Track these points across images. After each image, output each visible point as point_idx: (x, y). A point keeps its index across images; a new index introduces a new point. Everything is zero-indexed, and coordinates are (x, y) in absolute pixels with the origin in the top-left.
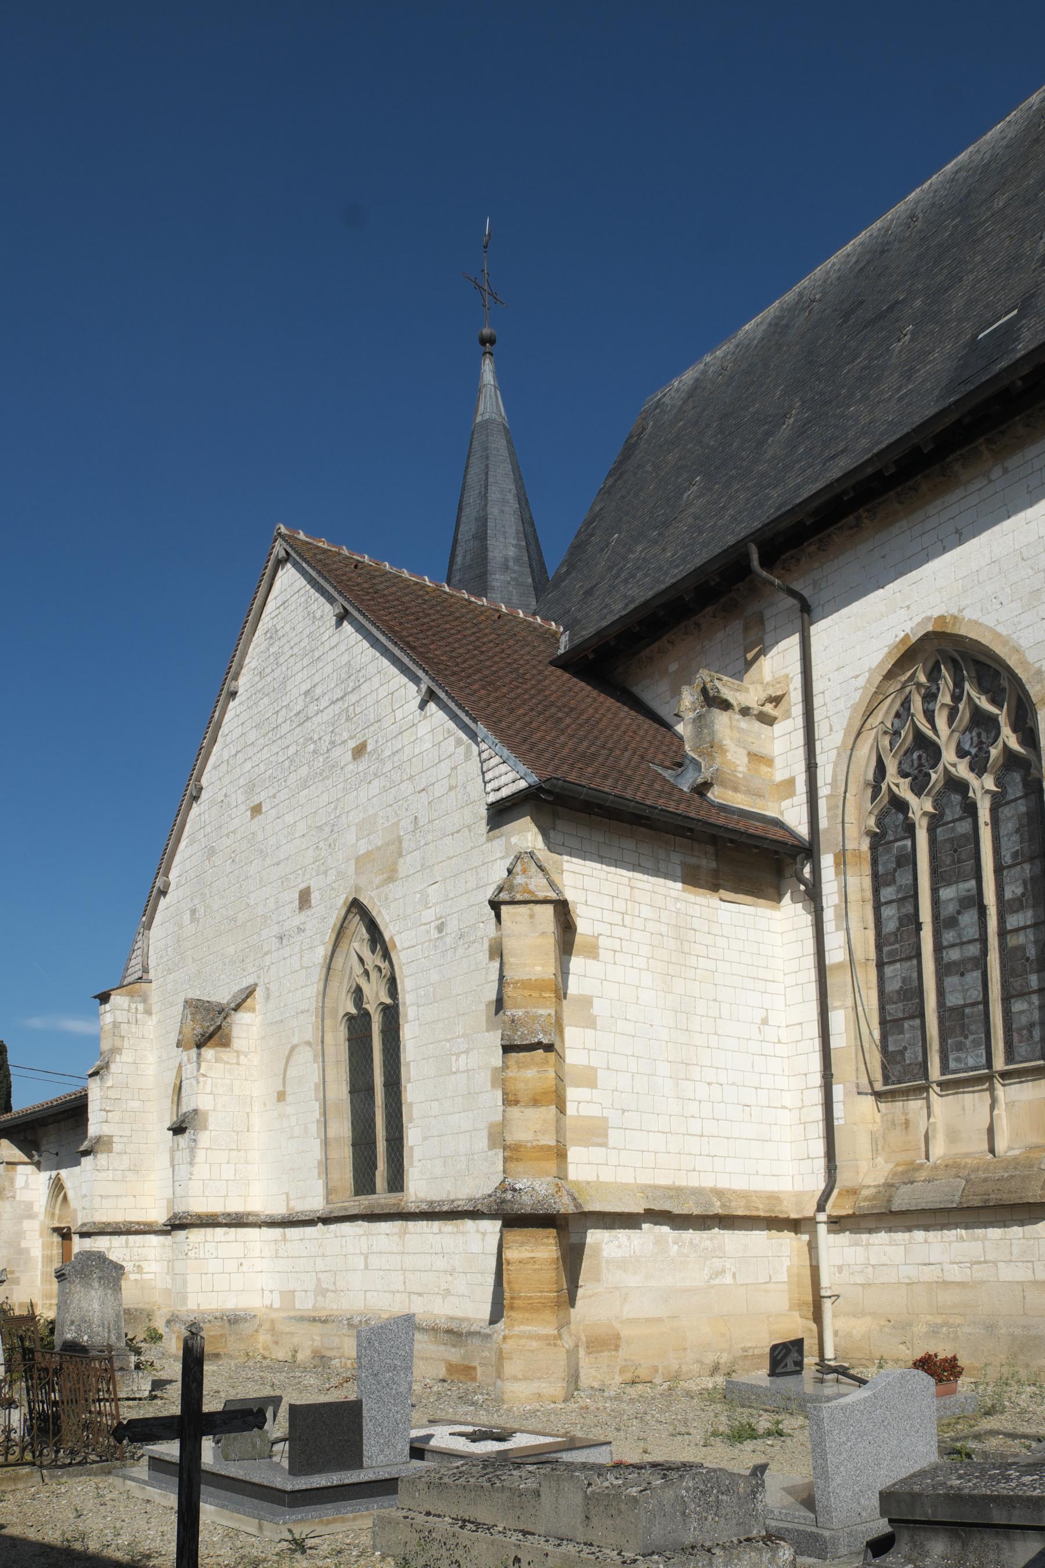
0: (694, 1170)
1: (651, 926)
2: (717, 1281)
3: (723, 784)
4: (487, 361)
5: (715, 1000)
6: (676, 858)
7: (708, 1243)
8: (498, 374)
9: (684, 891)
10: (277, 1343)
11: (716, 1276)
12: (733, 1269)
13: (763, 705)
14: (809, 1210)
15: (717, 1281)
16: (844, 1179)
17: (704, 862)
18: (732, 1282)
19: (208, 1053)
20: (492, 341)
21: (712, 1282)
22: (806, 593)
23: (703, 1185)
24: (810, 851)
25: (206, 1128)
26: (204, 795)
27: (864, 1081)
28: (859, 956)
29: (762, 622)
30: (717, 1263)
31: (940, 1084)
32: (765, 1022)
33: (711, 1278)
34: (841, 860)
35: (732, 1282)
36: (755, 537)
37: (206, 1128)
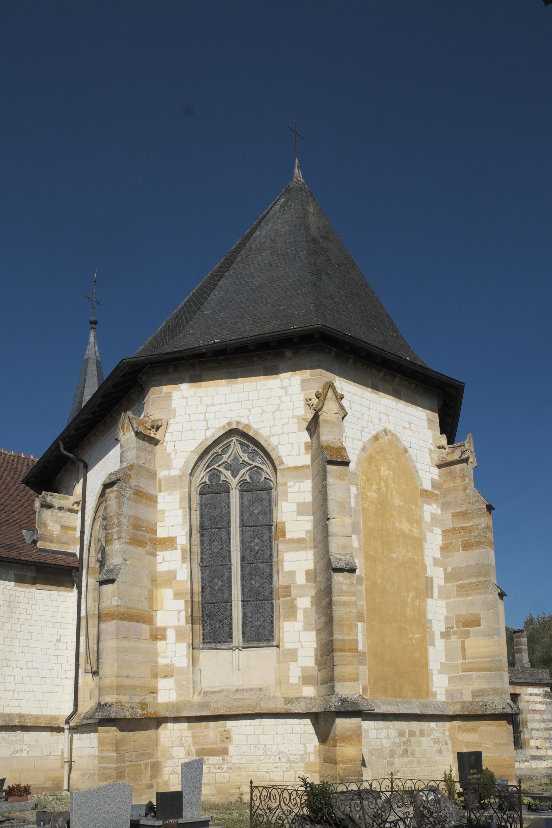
0: (8, 706)
2: (17, 755)
3: (44, 540)
4: (92, 332)
5: (29, 632)
6: (12, 573)
7: (13, 738)
8: (96, 337)
9: (15, 586)
11: (17, 753)
12: (28, 749)
13: (73, 505)
15: (17, 755)
17: (29, 574)
18: (26, 755)
20: (95, 323)
21: (14, 755)
22: (86, 461)
23: (13, 712)
24: (79, 569)
27: (89, 667)
30: (18, 747)
33: (13, 753)
35: (26, 755)
36: (62, 438)
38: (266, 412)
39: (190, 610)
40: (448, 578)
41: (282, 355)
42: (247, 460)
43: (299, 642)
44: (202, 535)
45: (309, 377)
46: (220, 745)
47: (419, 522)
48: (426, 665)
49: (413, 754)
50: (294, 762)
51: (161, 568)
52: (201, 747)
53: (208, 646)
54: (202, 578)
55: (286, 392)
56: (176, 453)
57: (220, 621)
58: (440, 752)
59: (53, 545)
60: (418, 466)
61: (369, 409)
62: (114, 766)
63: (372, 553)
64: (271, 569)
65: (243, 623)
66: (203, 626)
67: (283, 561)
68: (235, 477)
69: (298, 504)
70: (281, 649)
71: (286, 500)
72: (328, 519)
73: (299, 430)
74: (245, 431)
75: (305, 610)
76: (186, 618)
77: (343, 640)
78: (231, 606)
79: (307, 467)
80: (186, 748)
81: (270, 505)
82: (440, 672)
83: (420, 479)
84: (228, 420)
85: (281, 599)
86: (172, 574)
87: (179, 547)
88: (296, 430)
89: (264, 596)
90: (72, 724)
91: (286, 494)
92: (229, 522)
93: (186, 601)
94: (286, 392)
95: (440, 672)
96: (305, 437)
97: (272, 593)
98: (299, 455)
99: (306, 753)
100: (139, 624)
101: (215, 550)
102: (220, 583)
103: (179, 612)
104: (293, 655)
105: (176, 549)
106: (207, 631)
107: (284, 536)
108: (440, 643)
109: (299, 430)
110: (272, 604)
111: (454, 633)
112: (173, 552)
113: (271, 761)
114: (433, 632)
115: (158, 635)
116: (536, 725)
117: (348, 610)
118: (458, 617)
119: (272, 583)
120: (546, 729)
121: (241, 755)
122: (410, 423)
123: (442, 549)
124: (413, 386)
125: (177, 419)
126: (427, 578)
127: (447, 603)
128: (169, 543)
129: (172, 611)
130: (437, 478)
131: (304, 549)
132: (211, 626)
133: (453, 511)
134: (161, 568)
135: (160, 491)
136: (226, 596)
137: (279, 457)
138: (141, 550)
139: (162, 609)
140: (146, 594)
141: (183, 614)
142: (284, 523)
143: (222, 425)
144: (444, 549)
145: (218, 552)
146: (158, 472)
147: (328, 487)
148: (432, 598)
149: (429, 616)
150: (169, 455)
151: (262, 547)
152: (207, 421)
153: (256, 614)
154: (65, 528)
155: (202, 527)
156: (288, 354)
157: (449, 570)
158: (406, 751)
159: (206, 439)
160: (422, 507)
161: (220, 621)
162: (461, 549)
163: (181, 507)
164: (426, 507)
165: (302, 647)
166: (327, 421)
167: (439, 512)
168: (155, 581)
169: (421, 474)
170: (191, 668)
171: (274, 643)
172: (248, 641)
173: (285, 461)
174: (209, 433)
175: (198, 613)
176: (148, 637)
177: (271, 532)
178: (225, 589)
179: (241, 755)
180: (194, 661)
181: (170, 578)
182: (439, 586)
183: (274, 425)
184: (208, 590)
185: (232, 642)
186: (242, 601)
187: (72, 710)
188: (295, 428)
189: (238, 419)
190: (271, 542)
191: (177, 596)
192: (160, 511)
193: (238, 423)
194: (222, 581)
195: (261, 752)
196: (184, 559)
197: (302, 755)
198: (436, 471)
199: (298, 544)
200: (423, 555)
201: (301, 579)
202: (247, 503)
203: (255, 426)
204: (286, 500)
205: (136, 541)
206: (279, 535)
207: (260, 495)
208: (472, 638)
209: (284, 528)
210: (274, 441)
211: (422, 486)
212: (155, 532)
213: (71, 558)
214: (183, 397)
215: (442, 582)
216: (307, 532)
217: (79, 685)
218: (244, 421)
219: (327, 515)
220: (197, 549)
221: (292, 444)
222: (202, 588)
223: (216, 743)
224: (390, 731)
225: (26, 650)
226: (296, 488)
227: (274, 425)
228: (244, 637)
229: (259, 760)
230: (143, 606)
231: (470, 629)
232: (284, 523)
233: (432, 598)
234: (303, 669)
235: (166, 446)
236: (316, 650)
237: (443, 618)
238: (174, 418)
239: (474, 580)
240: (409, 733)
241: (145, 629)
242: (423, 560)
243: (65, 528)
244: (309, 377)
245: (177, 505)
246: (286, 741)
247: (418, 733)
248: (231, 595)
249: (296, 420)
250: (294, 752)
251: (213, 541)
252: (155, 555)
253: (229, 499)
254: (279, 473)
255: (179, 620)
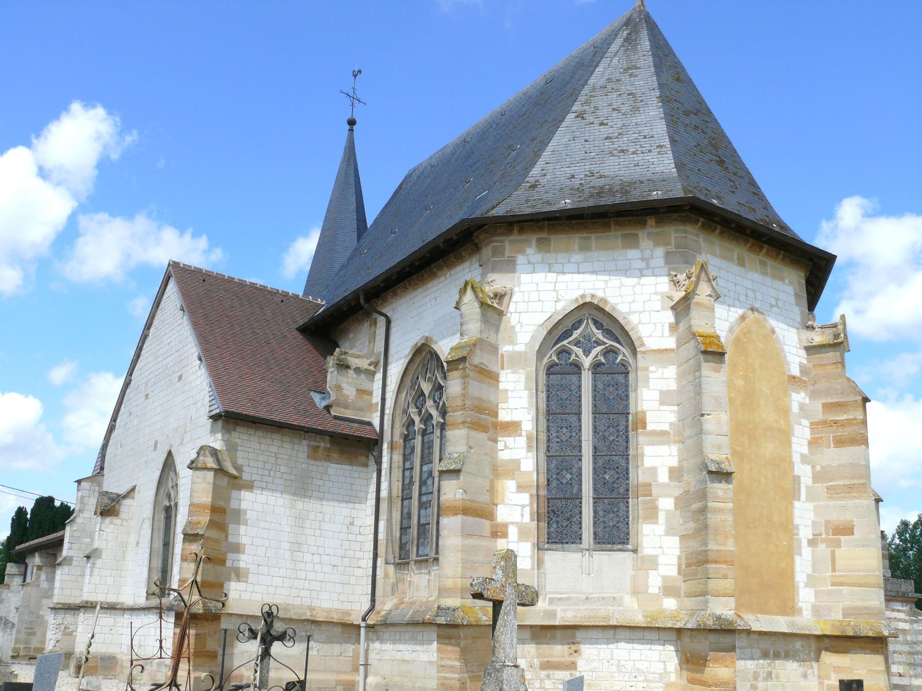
1: (285, 476)
3: (338, 405)
10: (79, 668)
14: (358, 621)
16: (377, 607)
17: (322, 444)
19: (108, 520)
22: (389, 315)
25: (100, 558)
26: (132, 384)
27: (391, 557)
28: (394, 494)
29: (376, 324)
31: (416, 561)
32: (352, 524)
34: (392, 447)
37: (100, 558)
38: (624, 285)
39: (535, 505)
40: (816, 477)
41: (643, 224)
42: (602, 338)
43: (661, 547)
44: (548, 420)
45: (674, 250)
46: (567, 659)
47: (785, 412)
48: (792, 577)
49: (777, 677)
50: (652, 681)
51: (504, 455)
52: (546, 659)
53: (554, 546)
54: (548, 469)
55: (648, 264)
56: (522, 326)
57: (568, 519)
58: (805, 676)
59: (348, 411)
60: (786, 348)
61: (735, 284)
62: (457, 676)
63: (739, 449)
64: (628, 463)
65: (595, 523)
66: (548, 523)
67: (643, 454)
68: (587, 356)
69: (661, 392)
70: (639, 555)
71: (648, 387)
72: (703, 415)
73: (663, 309)
74: (601, 305)
75: (667, 512)
76: (531, 514)
77: (718, 551)
78: (581, 503)
79: (672, 350)
80: (528, 660)
81: (627, 390)
82: (806, 585)
83: (788, 363)
84: (581, 292)
85: (640, 499)
86: (516, 463)
87: (524, 433)
88: (659, 309)
89: (619, 494)
90: (370, 622)
91: (647, 380)
92: (580, 406)
93: (531, 495)
94: (648, 264)
95: (806, 585)
96: (670, 317)
97: (628, 490)
98: (663, 336)
99: (666, 672)
100: (481, 520)
101: (564, 438)
102: (569, 476)
103: (523, 506)
104: (652, 563)
105: (520, 435)
106: (552, 529)
107: (644, 427)
108: (806, 551)
109: (663, 309)
110: (627, 502)
111: (823, 541)
112: (517, 439)
113: (626, 678)
114: (800, 539)
115: (499, 532)
116: (898, 647)
117: (723, 517)
118: (827, 523)
119: (628, 479)
120: (910, 653)
121: (591, 671)
122: (777, 300)
123: (810, 443)
124: (781, 257)
125: (523, 288)
126: (794, 476)
127: (815, 506)
128: (512, 428)
129: (516, 507)
130: (805, 361)
131: (668, 443)
132: (558, 523)
133: (824, 401)
134: (504, 455)
135: (503, 368)
136: (575, 491)
137: (640, 338)
138: (484, 436)
139: (503, 503)
140: (487, 483)
141: (527, 509)
142: (644, 412)
143: (574, 297)
144: (813, 443)
145: (567, 441)
146: (500, 347)
147: (703, 379)
148: (799, 500)
149: (797, 521)
150: (513, 327)
151: (617, 437)
152: (557, 292)
153: (609, 513)
154: (361, 392)
155: (549, 413)
156: (651, 222)
157: (818, 468)
158: (770, 674)
159: (556, 313)
160: (790, 396)
161: (568, 519)
162: (832, 445)
163: (526, 388)
164: (794, 396)
165: (663, 554)
166: (698, 304)
167: (807, 400)
168: (498, 471)
169: (790, 358)
170: (536, 571)
171: (630, 547)
172: (599, 543)
173: (646, 343)
174: (560, 306)
175: (544, 510)
176: (489, 534)
177: (627, 421)
178: (574, 483)
179: (591, 671)
180: (540, 563)
181: (512, 469)
182: (807, 487)
183: (634, 301)
184: (554, 484)
185: (581, 543)
186: (594, 498)
187: (366, 606)
188: (658, 305)
189: (593, 292)
190: (627, 432)
191: (521, 488)
192: (502, 390)
193: (593, 296)
194: (571, 474)
195: (614, 668)
196: (529, 447)
197: (661, 674)
198: (803, 353)
199: (661, 437)
200: (790, 451)
201: (663, 477)
202: (600, 386)
203: (612, 300)
204: (648, 387)
205: (477, 426)
206: (639, 425)
207: (616, 379)
208: (843, 548)
209: (645, 418)
210: (634, 319)
211: (789, 371)
212: (496, 415)
213: (368, 427)
214: (529, 263)
215: (809, 482)
216: (671, 424)
217: (378, 577)
218: (600, 294)
219: (701, 410)
220: (543, 437)
221: (655, 324)
222: (548, 480)
223: (563, 656)
224: (754, 650)
225: (318, 532)
226: (659, 374)
227: (634, 301)
228: (595, 539)
229: (613, 677)
230: (485, 498)
231: (842, 538)
232: (644, 412)
233: (799, 500)
234: (664, 578)
235: (510, 318)
236: (679, 558)
237: (809, 523)
238: (519, 286)
239: (847, 482)
240: (774, 654)
241: (487, 523)
242: (791, 456)
243: (361, 392)
244: (674, 250)
245: (522, 385)
246: (643, 658)
247: (783, 654)
248: (581, 490)
249: (659, 297)
250: (652, 670)
251: (562, 428)
252: (496, 441)
253: (580, 380)
254: (639, 356)
255: (522, 515)
